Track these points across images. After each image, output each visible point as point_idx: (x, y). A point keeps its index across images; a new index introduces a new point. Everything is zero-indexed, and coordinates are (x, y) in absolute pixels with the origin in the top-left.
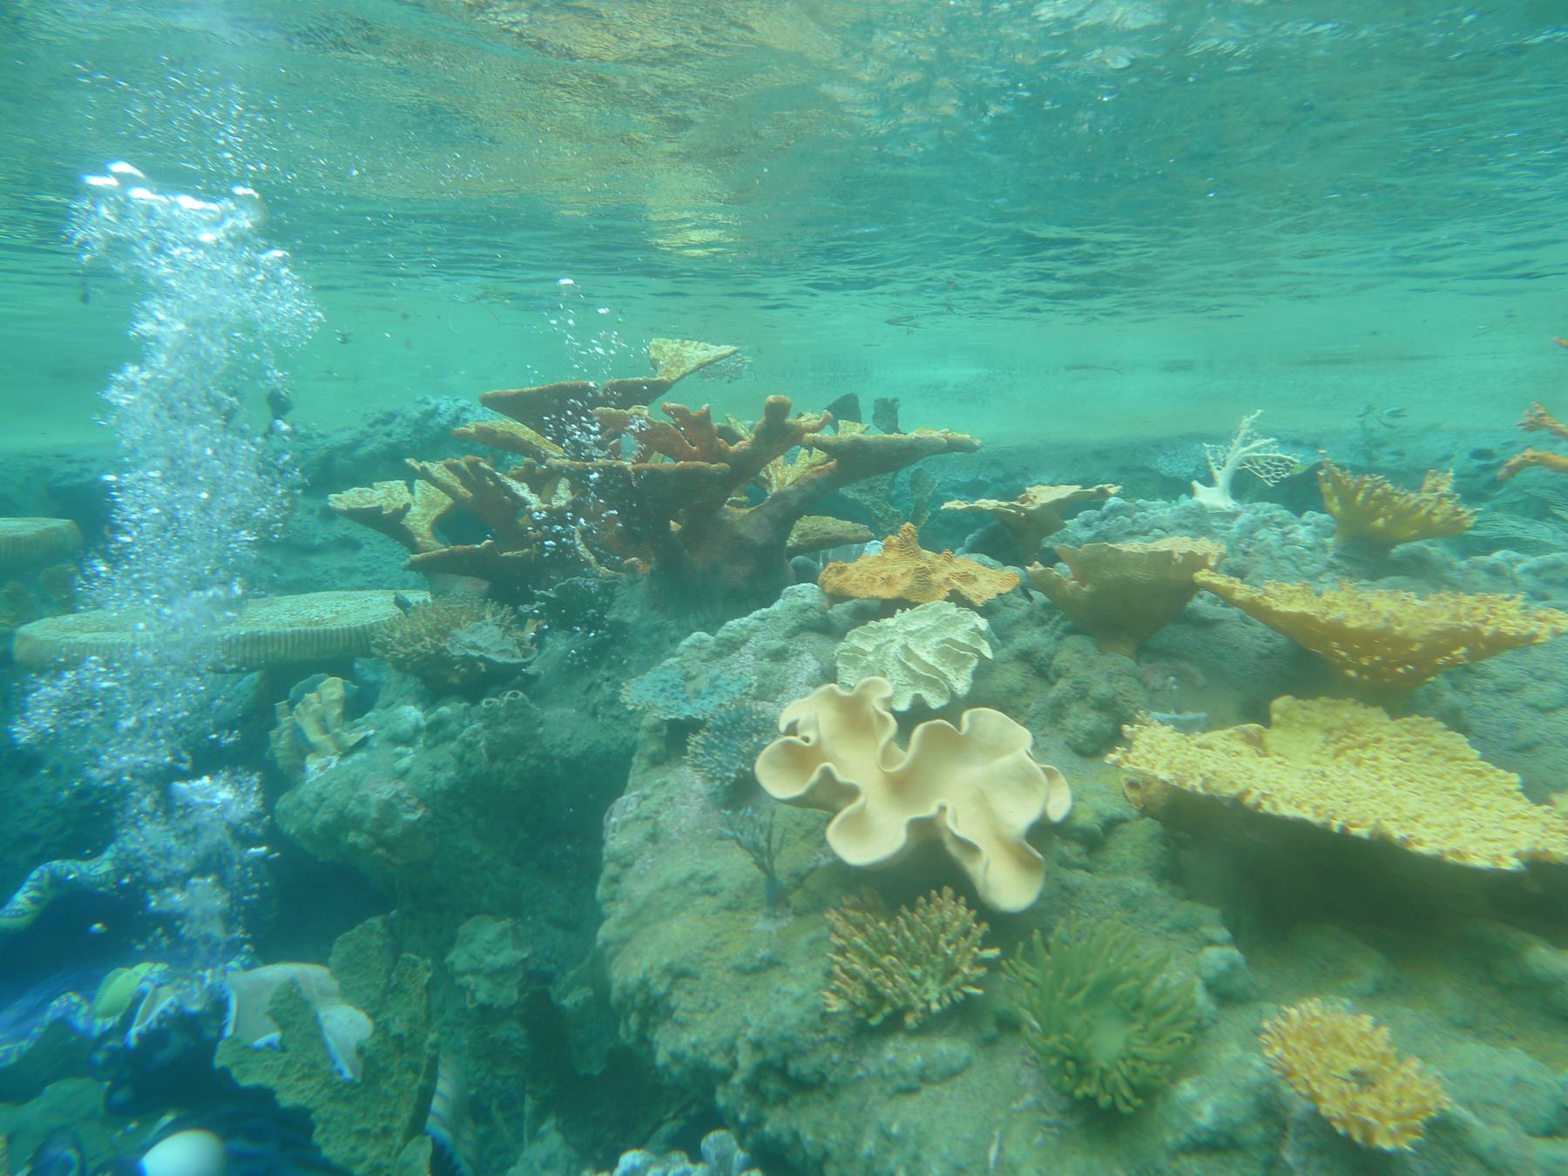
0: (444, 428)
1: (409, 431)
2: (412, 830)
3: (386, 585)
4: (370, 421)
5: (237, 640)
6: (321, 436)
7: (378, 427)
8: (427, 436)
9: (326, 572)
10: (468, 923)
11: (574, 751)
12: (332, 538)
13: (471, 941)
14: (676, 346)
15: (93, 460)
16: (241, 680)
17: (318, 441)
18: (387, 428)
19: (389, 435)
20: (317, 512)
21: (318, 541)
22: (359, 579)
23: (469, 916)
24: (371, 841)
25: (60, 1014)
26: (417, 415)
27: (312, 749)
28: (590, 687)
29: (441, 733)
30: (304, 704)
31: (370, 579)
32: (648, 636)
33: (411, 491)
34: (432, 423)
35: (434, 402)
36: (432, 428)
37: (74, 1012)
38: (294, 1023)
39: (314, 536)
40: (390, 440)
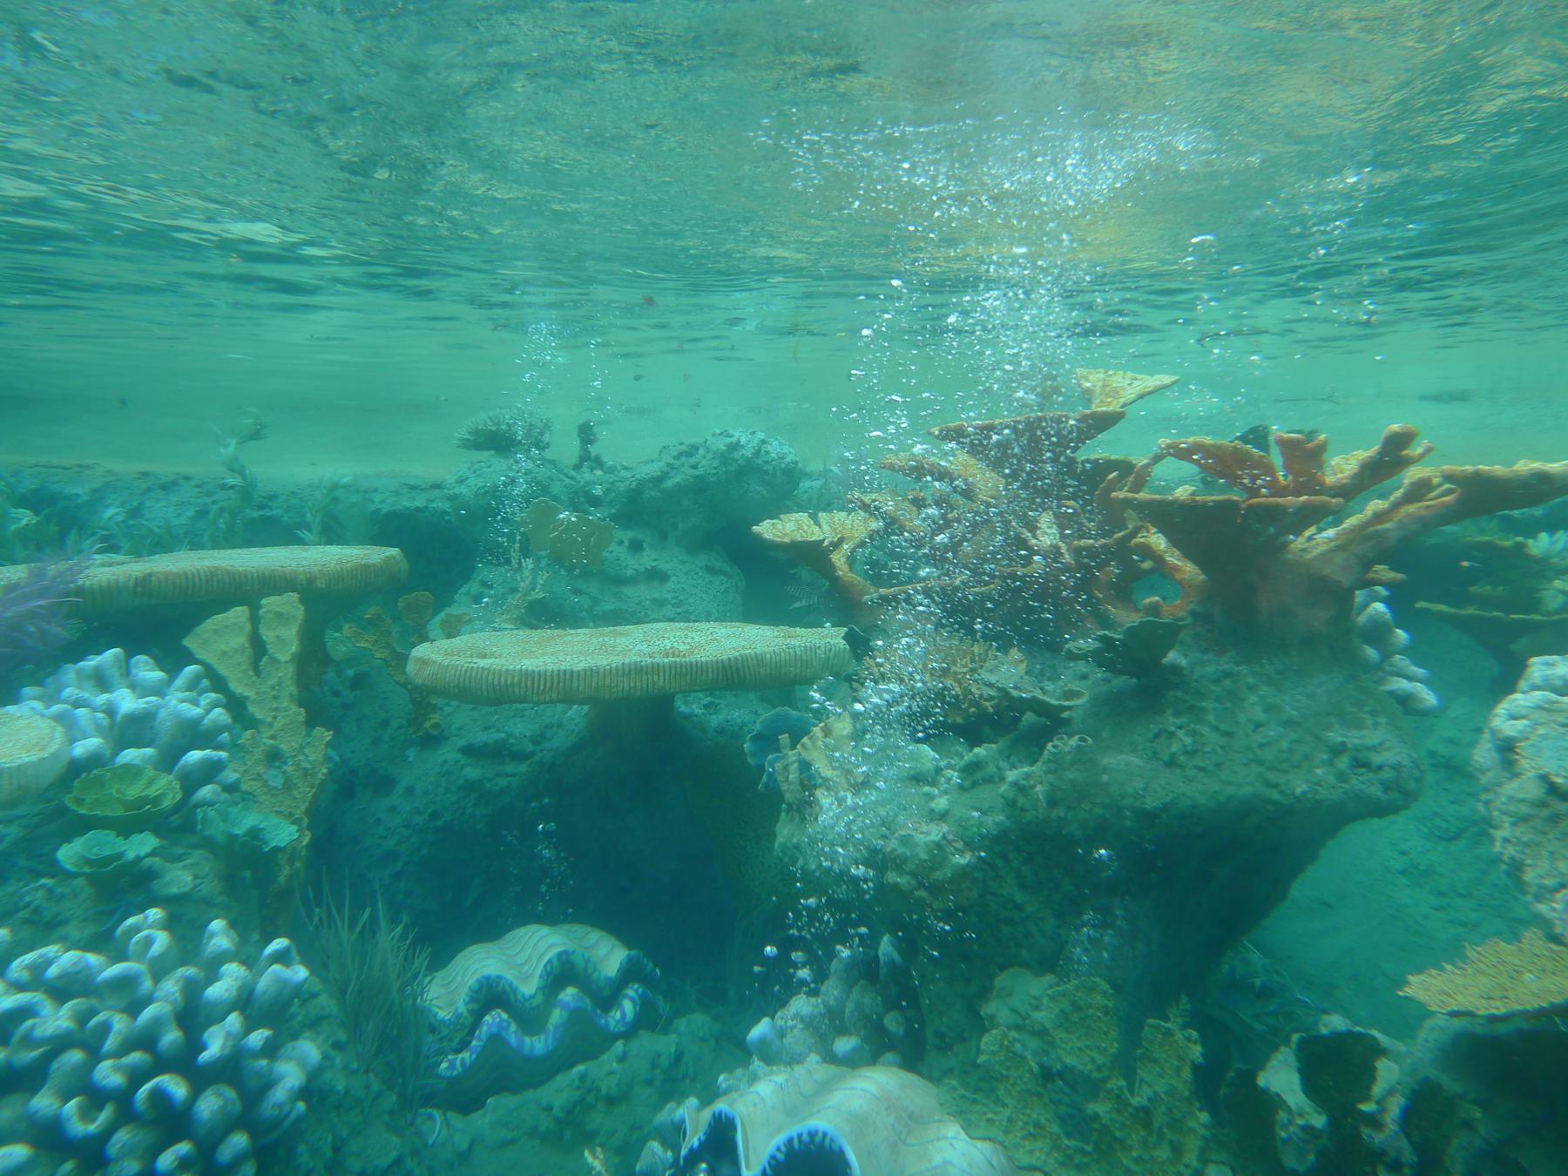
0: (748, 460)
1: (716, 463)
2: (962, 873)
3: (693, 617)
4: (676, 453)
5: (623, 669)
6: (626, 468)
7: (683, 459)
8: (731, 468)
9: (639, 603)
10: (1006, 974)
11: (1151, 803)
12: (642, 569)
13: (1010, 995)
14: (1101, 376)
15: (376, 490)
16: (570, 709)
17: (627, 474)
18: (692, 460)
19: (695, 467)
20: (626, 543)
21: (629, 572)
22: (669, 611)
23: (1002, 968)
24: (913, 882)
25: (495, 1030)
26: (723, 448)
27: (827, 784)
28: (1157, 735)
29: (979, 775)
30: (811, 738)
31: (679, 610)
32: (1217, 681)
33: (817, 523)
34: (736, 455)
35: (736, 434)
36: (737, 460)
37: (506, 1029)
38: (1008, 1077)
39: (626, 567)
40: (696, 472)
